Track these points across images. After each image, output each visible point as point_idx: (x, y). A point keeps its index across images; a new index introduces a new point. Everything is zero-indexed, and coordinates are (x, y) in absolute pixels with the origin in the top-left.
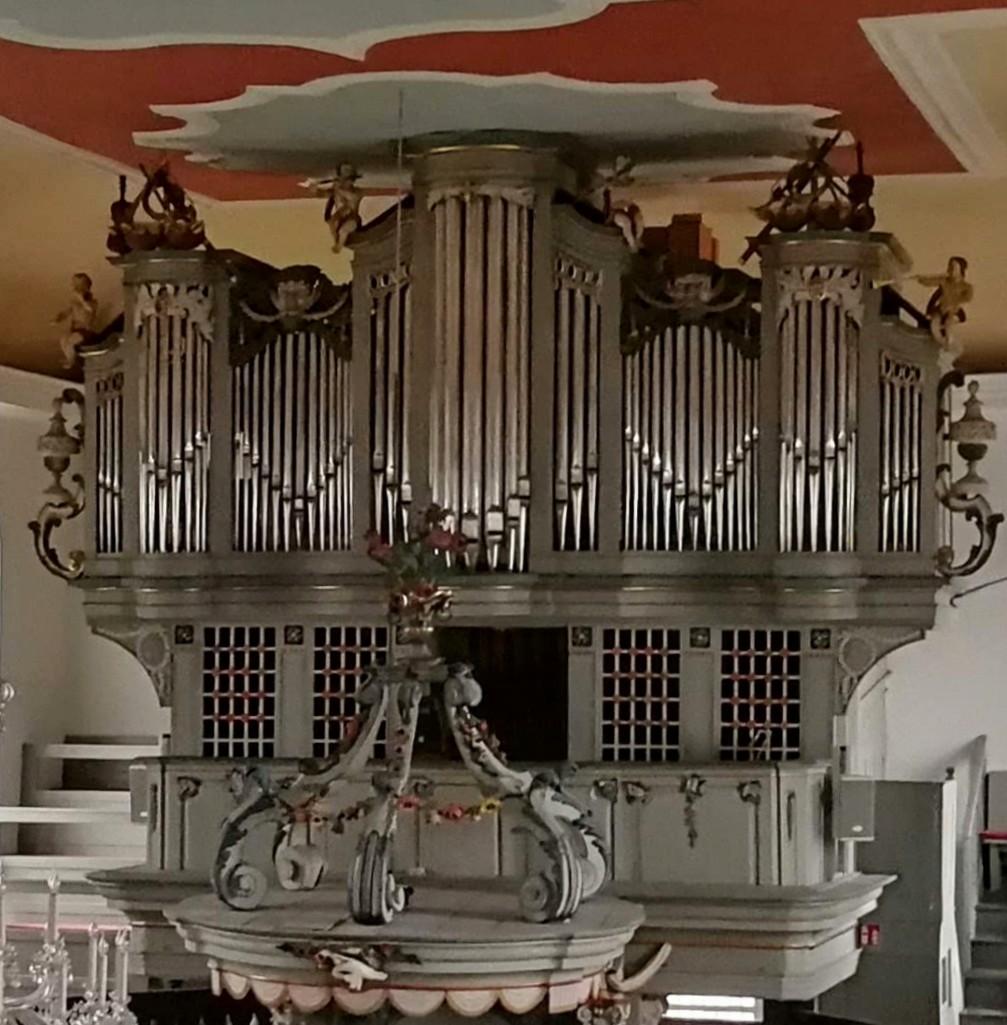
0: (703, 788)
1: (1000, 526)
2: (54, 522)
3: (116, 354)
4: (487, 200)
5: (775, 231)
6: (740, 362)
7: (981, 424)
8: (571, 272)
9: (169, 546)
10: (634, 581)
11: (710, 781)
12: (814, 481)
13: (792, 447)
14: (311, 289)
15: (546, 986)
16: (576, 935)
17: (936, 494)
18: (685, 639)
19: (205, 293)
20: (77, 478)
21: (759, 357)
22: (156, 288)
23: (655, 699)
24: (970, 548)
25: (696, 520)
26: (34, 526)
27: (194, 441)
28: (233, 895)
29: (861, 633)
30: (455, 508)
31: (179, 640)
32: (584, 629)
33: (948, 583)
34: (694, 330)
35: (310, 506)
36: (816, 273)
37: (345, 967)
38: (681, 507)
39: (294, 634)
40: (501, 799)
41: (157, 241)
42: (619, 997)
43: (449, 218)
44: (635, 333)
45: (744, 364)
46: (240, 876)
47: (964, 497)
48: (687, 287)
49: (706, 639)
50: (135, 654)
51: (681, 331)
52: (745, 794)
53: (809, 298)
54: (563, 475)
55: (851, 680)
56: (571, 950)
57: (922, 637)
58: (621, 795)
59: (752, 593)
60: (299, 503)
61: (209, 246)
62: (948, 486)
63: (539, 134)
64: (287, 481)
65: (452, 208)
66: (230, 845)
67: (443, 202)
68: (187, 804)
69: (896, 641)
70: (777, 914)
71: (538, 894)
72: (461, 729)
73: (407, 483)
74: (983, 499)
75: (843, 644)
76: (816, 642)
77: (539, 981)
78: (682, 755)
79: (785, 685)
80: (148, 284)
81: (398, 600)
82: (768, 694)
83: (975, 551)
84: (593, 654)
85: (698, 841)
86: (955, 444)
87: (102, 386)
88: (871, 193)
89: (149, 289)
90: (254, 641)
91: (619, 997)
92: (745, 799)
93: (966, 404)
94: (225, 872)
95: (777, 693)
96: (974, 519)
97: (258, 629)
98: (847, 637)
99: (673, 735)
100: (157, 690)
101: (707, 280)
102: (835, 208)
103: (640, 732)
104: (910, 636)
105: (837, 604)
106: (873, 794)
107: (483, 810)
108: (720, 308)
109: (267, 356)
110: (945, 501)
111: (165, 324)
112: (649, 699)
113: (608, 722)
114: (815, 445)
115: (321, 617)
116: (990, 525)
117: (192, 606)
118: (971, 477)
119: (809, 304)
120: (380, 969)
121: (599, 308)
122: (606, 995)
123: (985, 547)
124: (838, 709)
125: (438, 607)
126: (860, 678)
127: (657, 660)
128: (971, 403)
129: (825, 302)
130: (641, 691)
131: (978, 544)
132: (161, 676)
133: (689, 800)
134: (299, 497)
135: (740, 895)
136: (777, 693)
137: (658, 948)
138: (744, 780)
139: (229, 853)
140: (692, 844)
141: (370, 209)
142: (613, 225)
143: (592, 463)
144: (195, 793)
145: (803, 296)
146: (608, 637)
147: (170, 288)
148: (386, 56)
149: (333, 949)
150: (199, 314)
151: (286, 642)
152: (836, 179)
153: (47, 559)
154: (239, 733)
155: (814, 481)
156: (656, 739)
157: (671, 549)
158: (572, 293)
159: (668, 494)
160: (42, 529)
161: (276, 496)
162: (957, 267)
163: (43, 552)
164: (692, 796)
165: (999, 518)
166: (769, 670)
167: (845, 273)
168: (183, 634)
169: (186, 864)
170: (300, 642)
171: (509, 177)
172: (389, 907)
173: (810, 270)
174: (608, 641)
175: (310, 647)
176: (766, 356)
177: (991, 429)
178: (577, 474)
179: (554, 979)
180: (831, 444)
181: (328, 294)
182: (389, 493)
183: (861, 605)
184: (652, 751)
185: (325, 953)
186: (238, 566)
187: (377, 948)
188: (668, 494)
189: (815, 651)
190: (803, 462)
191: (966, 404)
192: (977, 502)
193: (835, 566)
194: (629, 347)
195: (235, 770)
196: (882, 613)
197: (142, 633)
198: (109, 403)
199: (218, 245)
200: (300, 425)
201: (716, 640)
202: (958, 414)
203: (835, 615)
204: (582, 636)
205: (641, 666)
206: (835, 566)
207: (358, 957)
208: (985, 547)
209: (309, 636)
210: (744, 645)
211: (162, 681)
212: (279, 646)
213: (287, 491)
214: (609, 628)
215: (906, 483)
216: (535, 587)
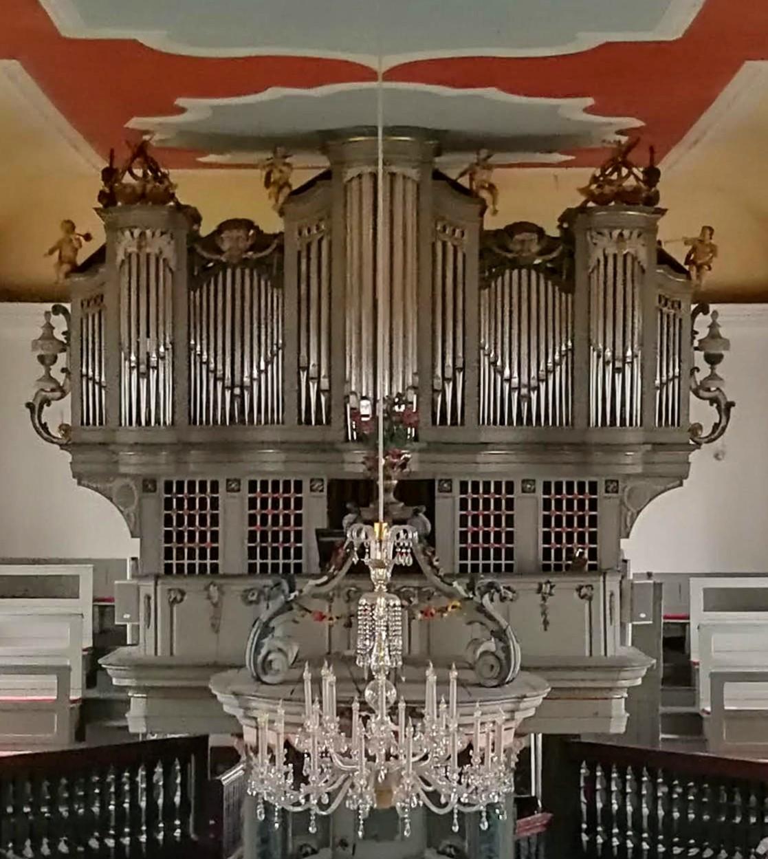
0: (553, 591)
1: (732, 409)
3: (97, 278)
5: (591, 204)
6: (557, 295)
7: (719, 340)
8: (444, 230)
9: (148, 422)
10: (490, 447)
11: (558, 586)
12: (143, 383)
13: (602, 354)
14: (247, 235)
16: (528, 695)
17: (691, 388)
18: (518, 488)
19: (172, 238)
21: (573, 294)
22: (137, 232)
23: (497, 529)
24: (713, 424)
25: (526, 404)
26: (29, 405)
27: (165, 345)
28: (266, 673)
29: (640, 483)
30: (371, 395)
32: (447, 481)
33: (699, 448)
35: (246, 393)
36: (621, 235)
38: (515, 395)
39: (233, 485)
40: (460, 601)
41: (140, 197)
43: (364, 189)
44: (487, 274)
45: (561, 296)
46: (271, 661)
47: (708, 390)
48: (523, 242)
49: (528, 490)
50: (111, 500)
52: (582, 594)
53: (616, 252)
55: (632, 514)
57: (681, 485)
59: (572, 457)
60: (237, 391)
61: (178, 204)
62: (699, 383)
63: (425, 129)
65: (367, 184)
66: (264, 638)
67: (360, 176)
68: (175, 609)
69: (660, 488)
70: (615, 675)
71: (492, 667)
73: (324, 377)
74: (721, 391)
75: (627, 489)
76: (236, 488)
78: (515, 568)
79: (587, 518)
80: (131, 229)
82: (575, 525)
83: (716, 426)
84: (453, 498)
86: (702, 353)
87: (85, 304)
88: (658, 181)
89: (132, 234)
90: (287, 490)
92: (582, 597)
93: (710, 327)
94: (260, 658)
95: (581, 523)
96: (715, 405)
97: (501, 483)
98: (630, 485)
100: (129, 525)
101: (535, 236)
102: (636, 191)
103: (486, 552)
104: (671, 485)
105: (632, 462)
106: (652, 589)
107: (450, 609)
109: (212, 288)
110: (697, 394)
111: (143, 259)
112: (492, 529)
113: (464, 546)
115: (251, 473)
116: (726, 409)
117: (163, 467)
118: (713, 376)
119: (615, 256)
121: (464, 256)
124: (624, 534)
125: (403, 466)
126: (638, 513)
127: (497, 502)
128: (713, 326)
129: (625, 256)
130: (487, 524)
131: (717, 421)
132: (132, 515)
133: (544, 599)
134: (238, 386)
135: (579, 664)
136: (581, 523)
138: (582, 584)
139: (263, 644)
140: (546, 629)
141: (298, 179)
143: (460, 364)
144: (182, 600)
145: (611, 251)
146: (464, 485)
147: (148, 232)
148: (395, 74)
150: (169, 253)
151: (228, 491)
152: (635, 170)
153: (41, 430)
154: (191, 556)
155: (143, 383)
156: (498, 557)
157: (527, 424)
158: (444, 245)
159: (507, 386)
160: (34, 409)
161: (219, 385)
162: (708, 232)
163: (38, 425)
164: (546, 596)
165: (732, 404)
166: (576, 508)
168: (148, 485)
169: (175, 652)
170: (239, 490)
171: (409, 161)
173: (616, 233)
174: (252, 487)
176: (580, 294)
177: (726, 344)
180: (629, 353)
181: (262, 240)
182: (311, 384)
183: (646, 463)
184: (261, 564)
186: (195, 436)
188: (507, 386)
189: (607, 495)
190: (611, 365)
191: (710, 327)
192: (717, 393)
193: (631, 436)
194: (485, 283)
195: (211, 583)
196: (659, 469)
197: (118, 484)
198: (90, 319)
199: (183, 202)
200: (238, 333)
201: (540, 488)
202: (703, 333)
203: (629, 470)
204: (612, 486)
206: (631, 436)
209: (245, 486)
210: (559, 491)
211: (133, 519)
212: (222, 494)
213: (228, 382)
214: (298, 479)
215: (671, 380)
216: (421, 451)
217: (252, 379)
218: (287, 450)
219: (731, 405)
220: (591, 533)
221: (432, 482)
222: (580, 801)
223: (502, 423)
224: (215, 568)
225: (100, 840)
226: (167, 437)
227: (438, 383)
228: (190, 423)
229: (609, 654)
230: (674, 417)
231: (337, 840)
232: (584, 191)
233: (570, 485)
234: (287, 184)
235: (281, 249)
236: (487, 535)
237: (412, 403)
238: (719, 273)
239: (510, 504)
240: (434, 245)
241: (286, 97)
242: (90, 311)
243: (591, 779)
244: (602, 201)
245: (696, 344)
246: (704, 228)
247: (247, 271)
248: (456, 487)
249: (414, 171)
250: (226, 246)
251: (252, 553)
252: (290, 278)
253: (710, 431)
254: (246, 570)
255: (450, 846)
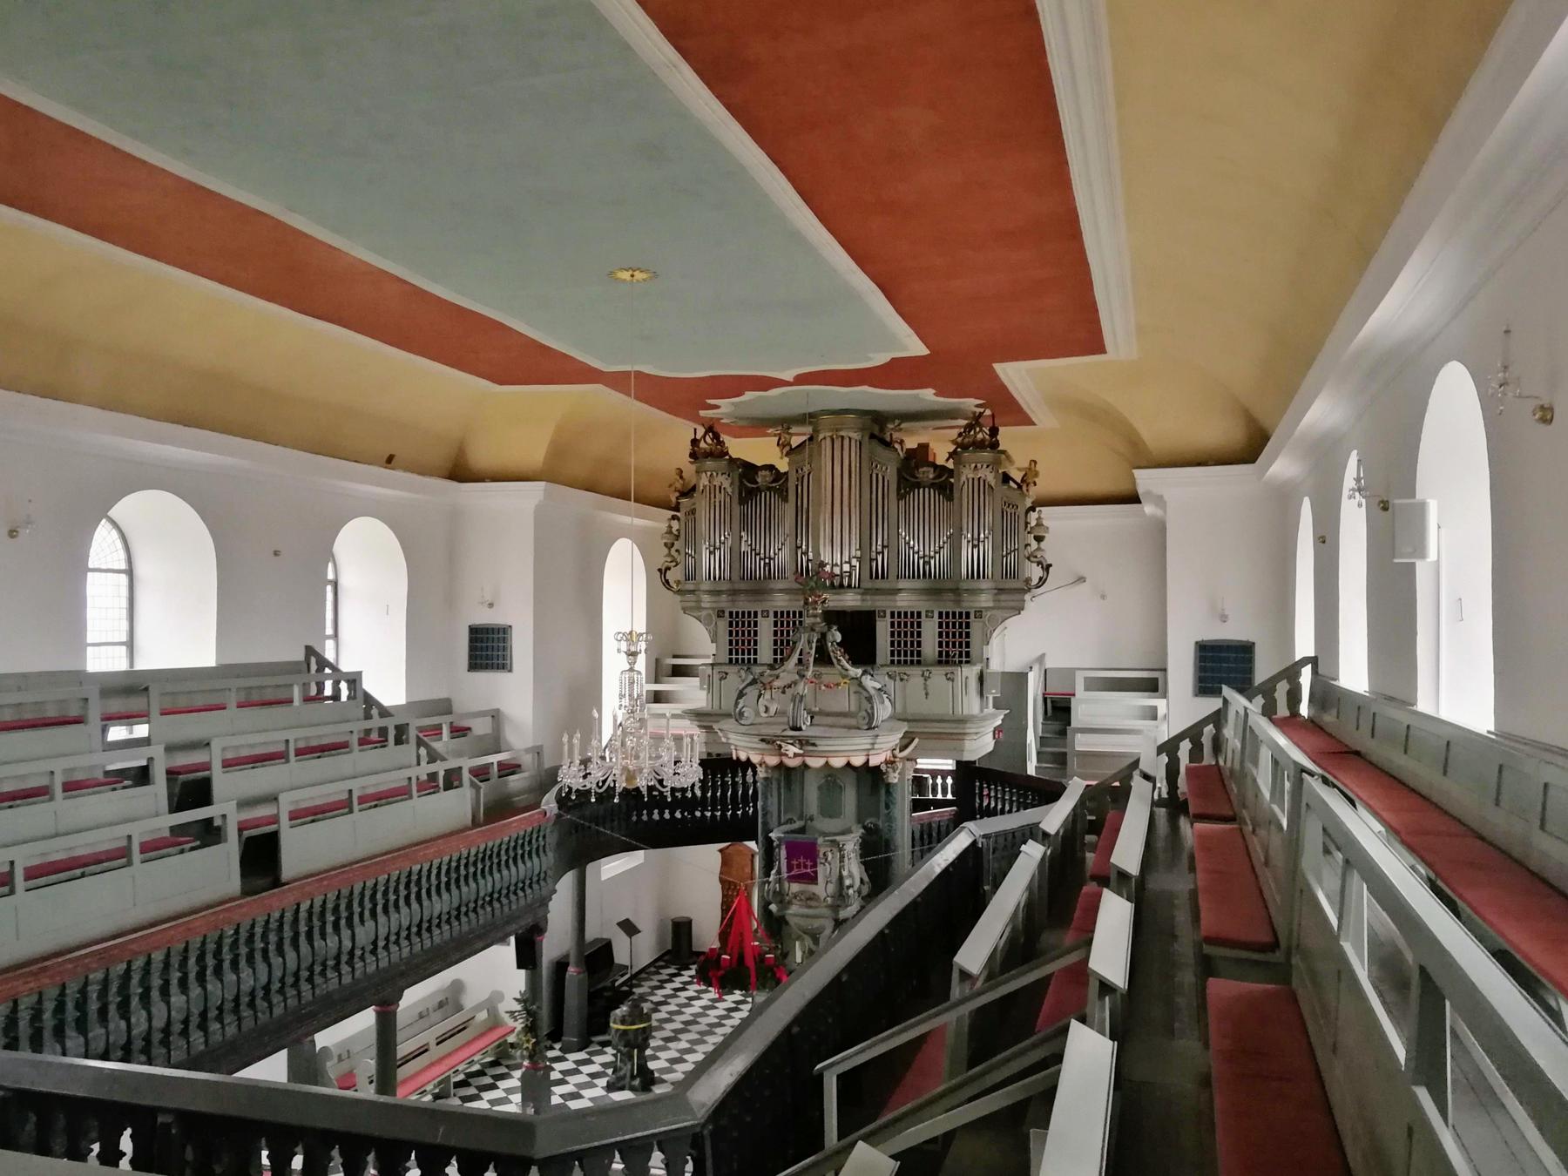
1: (1051, 568)
2: (668, 568)
4: (842, 437)
5: (959, 450)
8: (876, 467)
9: (715, 578)
11: (934, 672)
12: (976, 551)
15: (868, 755)
19: (729, 476)
20: (677, 551)
22: (709, 473)
26: (660, 570)
28: (742, 719)
29: (995, 612)
31: (719, 616)
34: (927, 490)
35: (772, 561)
36: (976, 466)
37: (786, 748)
38: (921, 561)
39: (766, 614)
41: (709, 455)
42: (897, 760)
47: (1036, 557)
48: (924, 472)
51: (921, 490)
54: (874, 548)
56: (878, 741)
57: (1019, 613)
58: (898, 678)
59: (951, 596)
60: (767, 561)
61: (730, 457)
64: (762, 552)
65: (828, 441)
67: (825, 438)
69: (1008, 615)
70: (961, 726)
72: (833, 652)
77: (865, 753)
81: (807, 599)
83: (1041, 579)
85: (929, 697)
91: (897, 760)
93: (1037, 519)
94: (738, 710)
99: (919, 654)
101: (932, 470)
102: (983, 440)
105: (985, 601)
108: (937, 481)
110: (1028, 558)
111: (712, 488)
112: (909, 639)
114: (976, 536)
115: (776, 607)
117: (724, 602)
118: (1039, 549)
119: (973, 479)
120: (801, 749)
122: (892, 759)
123: (1045, 577)
125: (824, 602)
128: (1039, 519)
129: (979, 479)
130: (906, 636)
133: (926, 680)
137: (913, 739)
141: (795, 441)
142: (894, 447)
143: (885, 544)
144: (726, 678)
145: (971, 476)
147: (715, 474)
148: (801, 380)
149: (782, 741)
150: (726, 484)
152: (984, 429)
155: (976, 551)
158: (877, 475)
159: (916, 556)
161: (758, 557)
162: (1033, 464)
165: (1050, 565)
167: (988, 466)
168: (720, 614)
171: (852, 428)
172: (804, 724)
173: (973, 465)
174: (941, 614)
175: (772, 619)
178: (880, 548)
179: (871, 752)
180: (982, 536)
181: (778, 476)
183: (994, 601)
185: (778, 742)
186: (743, 586)
187: (799, 740)
188: (916, 556)
193: (984, 584)
194: (900, 497)
196: (1003, 604)
197: (704, 613)
200: (768, 528)
201: (936, 615)
202: (1033, 523)
205: (906, 626)
207: (792, 744)
208: (1045, 577)
212: (759, 618)
217: (775, 554)
218: (713, 595)
219: (1050, 566)
220: (966, 642)
221: (875, 611)
222: (975, 801)
223: (914, 577)
224: (755, 660)
225: (702, 812)
226: (725, 586)
227: (874, 555)
228: (871, 577)
229: (964, 713)
230: (1012, 574)
231: (808, 817)
232: (954, 442)
233: (954, 613)
234: (789, 444)
235: (787, 479)
236: (906, 643)
237: (855, 566)
238: (1043, 486)
239: (919, 625)
240: (871, 476)
241: (760, 397)
242: (690, 518)
243: (981, 789)
244: (965, 447)
245: (1029, 529)
246: (1031, 461)
247: (932, 490)
248: (888, 615)
249: (856, 434)
250: (759, 480)
251: (731, 652)
252: (792, 497)
253: (1038, 581)
254: (727, 661)
255: (871, 823)
